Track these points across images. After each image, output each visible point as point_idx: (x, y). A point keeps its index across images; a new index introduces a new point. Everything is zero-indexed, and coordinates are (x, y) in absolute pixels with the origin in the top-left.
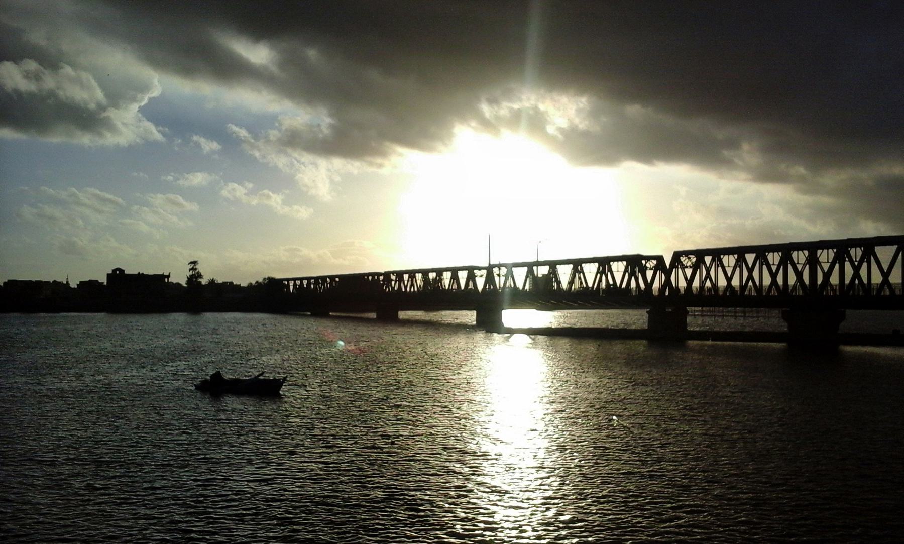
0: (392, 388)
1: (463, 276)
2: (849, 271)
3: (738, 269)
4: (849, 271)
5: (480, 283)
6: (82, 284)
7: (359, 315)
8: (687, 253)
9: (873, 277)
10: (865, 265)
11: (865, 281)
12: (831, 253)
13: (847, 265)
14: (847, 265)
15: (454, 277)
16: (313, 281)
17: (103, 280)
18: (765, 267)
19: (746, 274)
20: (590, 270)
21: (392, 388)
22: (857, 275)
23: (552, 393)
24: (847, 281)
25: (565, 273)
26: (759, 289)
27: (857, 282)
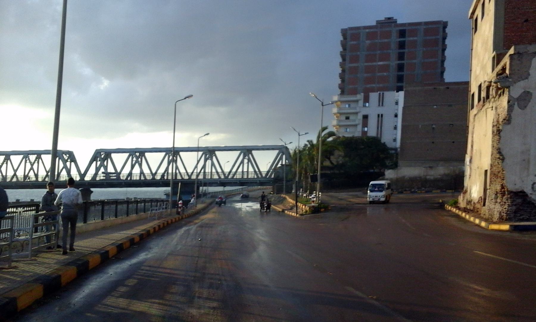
3: (24, 160)
19: (28, 166)
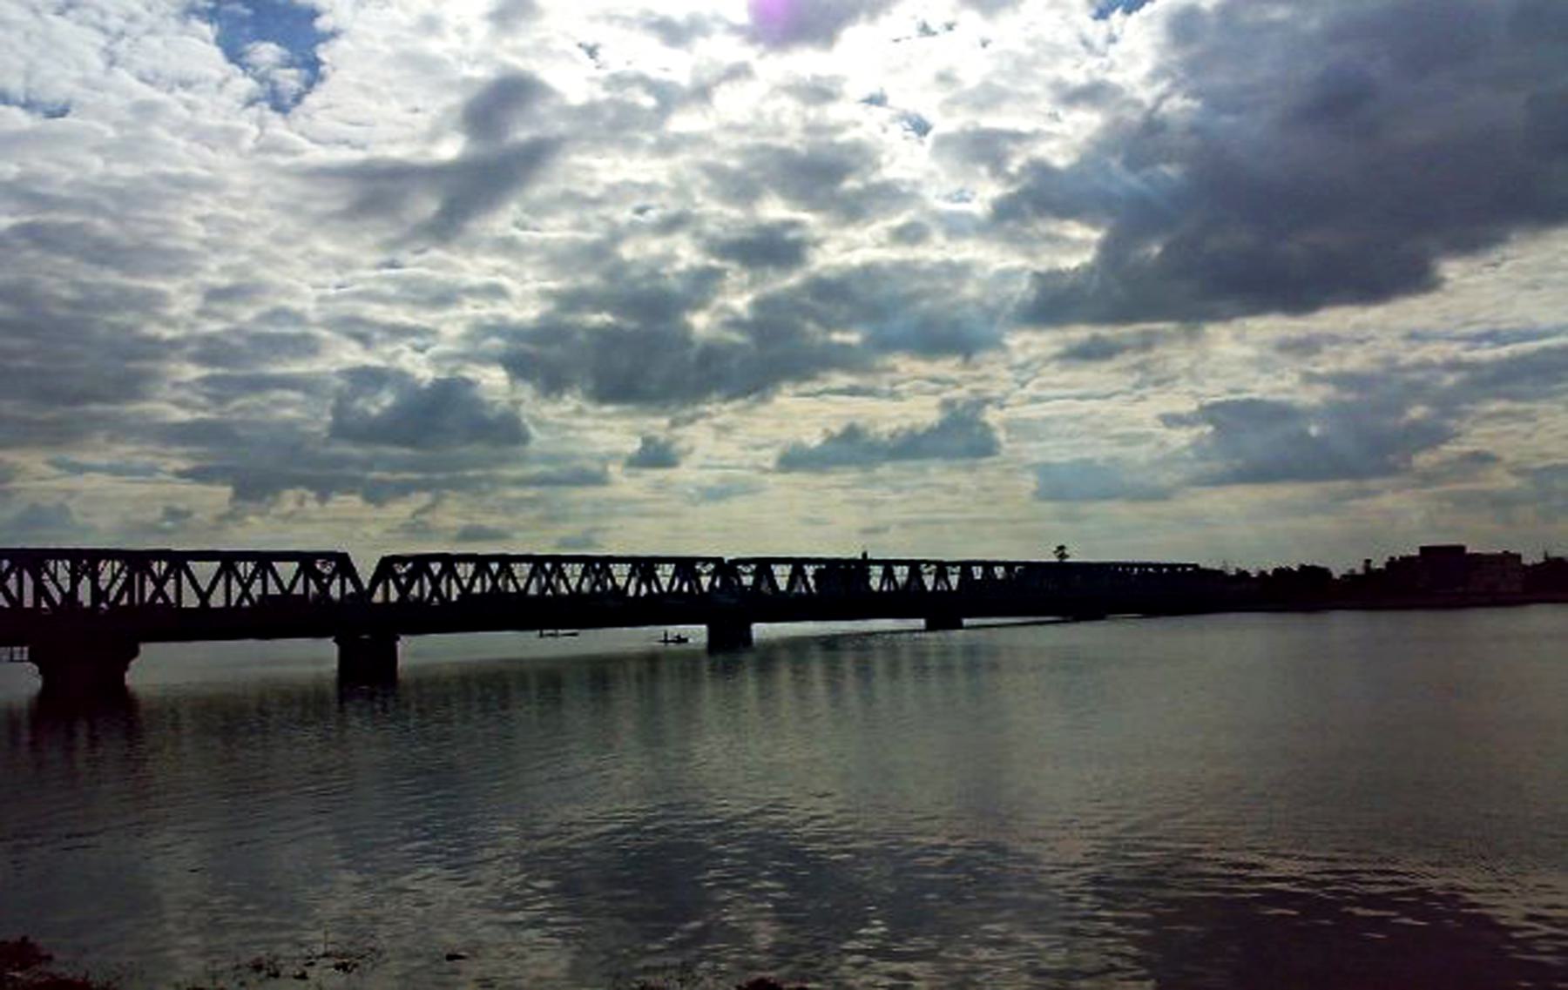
0: (980, 905)
1: (901, 573)
2: (150, 587)
4: (236, 590)
5: (954, 580)
6: (1392, 563)
7: (1504, 351)
8: (402, 560)
9: (184, 598)
10: (258, 582)
11: (172, 599)
12: (471, 568)
13: (234, 582)
14: (234, 582)
15: (888, 575)
16: (810, 570)
17: (1416, 553)
18: (453, 581)
20: (665, 573)
21: (980, 905)
22: (159, 591)
23: (418, 929)
24: (147, 599)
25: (782, 575)
26: (445, 601)
27: (44, 605)
